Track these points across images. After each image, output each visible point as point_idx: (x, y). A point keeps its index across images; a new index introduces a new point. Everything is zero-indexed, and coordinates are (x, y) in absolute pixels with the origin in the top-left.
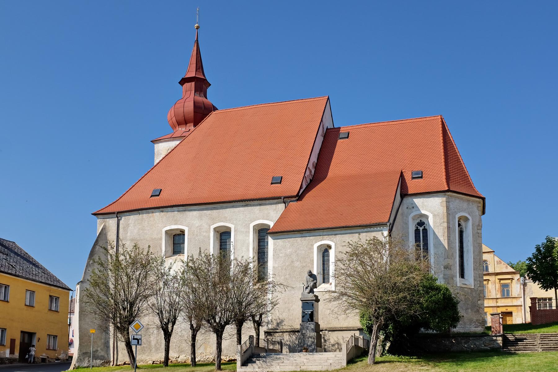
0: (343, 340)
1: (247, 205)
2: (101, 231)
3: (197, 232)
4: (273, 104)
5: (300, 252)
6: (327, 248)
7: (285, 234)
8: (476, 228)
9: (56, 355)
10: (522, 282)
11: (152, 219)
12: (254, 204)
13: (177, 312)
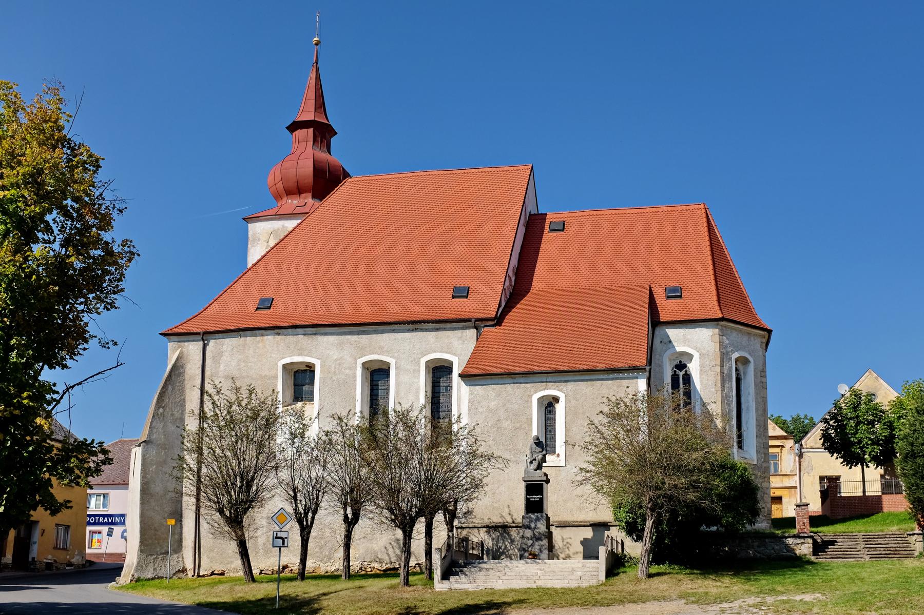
0: (563, 542)
1: (416, 329)
2: (176, 361)
3: (335, 368)
4: (446, 172)
5: (510, 406)
6: (552, 400)
7: (487, 378)
8: (759, 375)
9: (68, 557)
10: (797, 451)
11: (261, 345)
12: (427, 328)
13: (321, 493)
